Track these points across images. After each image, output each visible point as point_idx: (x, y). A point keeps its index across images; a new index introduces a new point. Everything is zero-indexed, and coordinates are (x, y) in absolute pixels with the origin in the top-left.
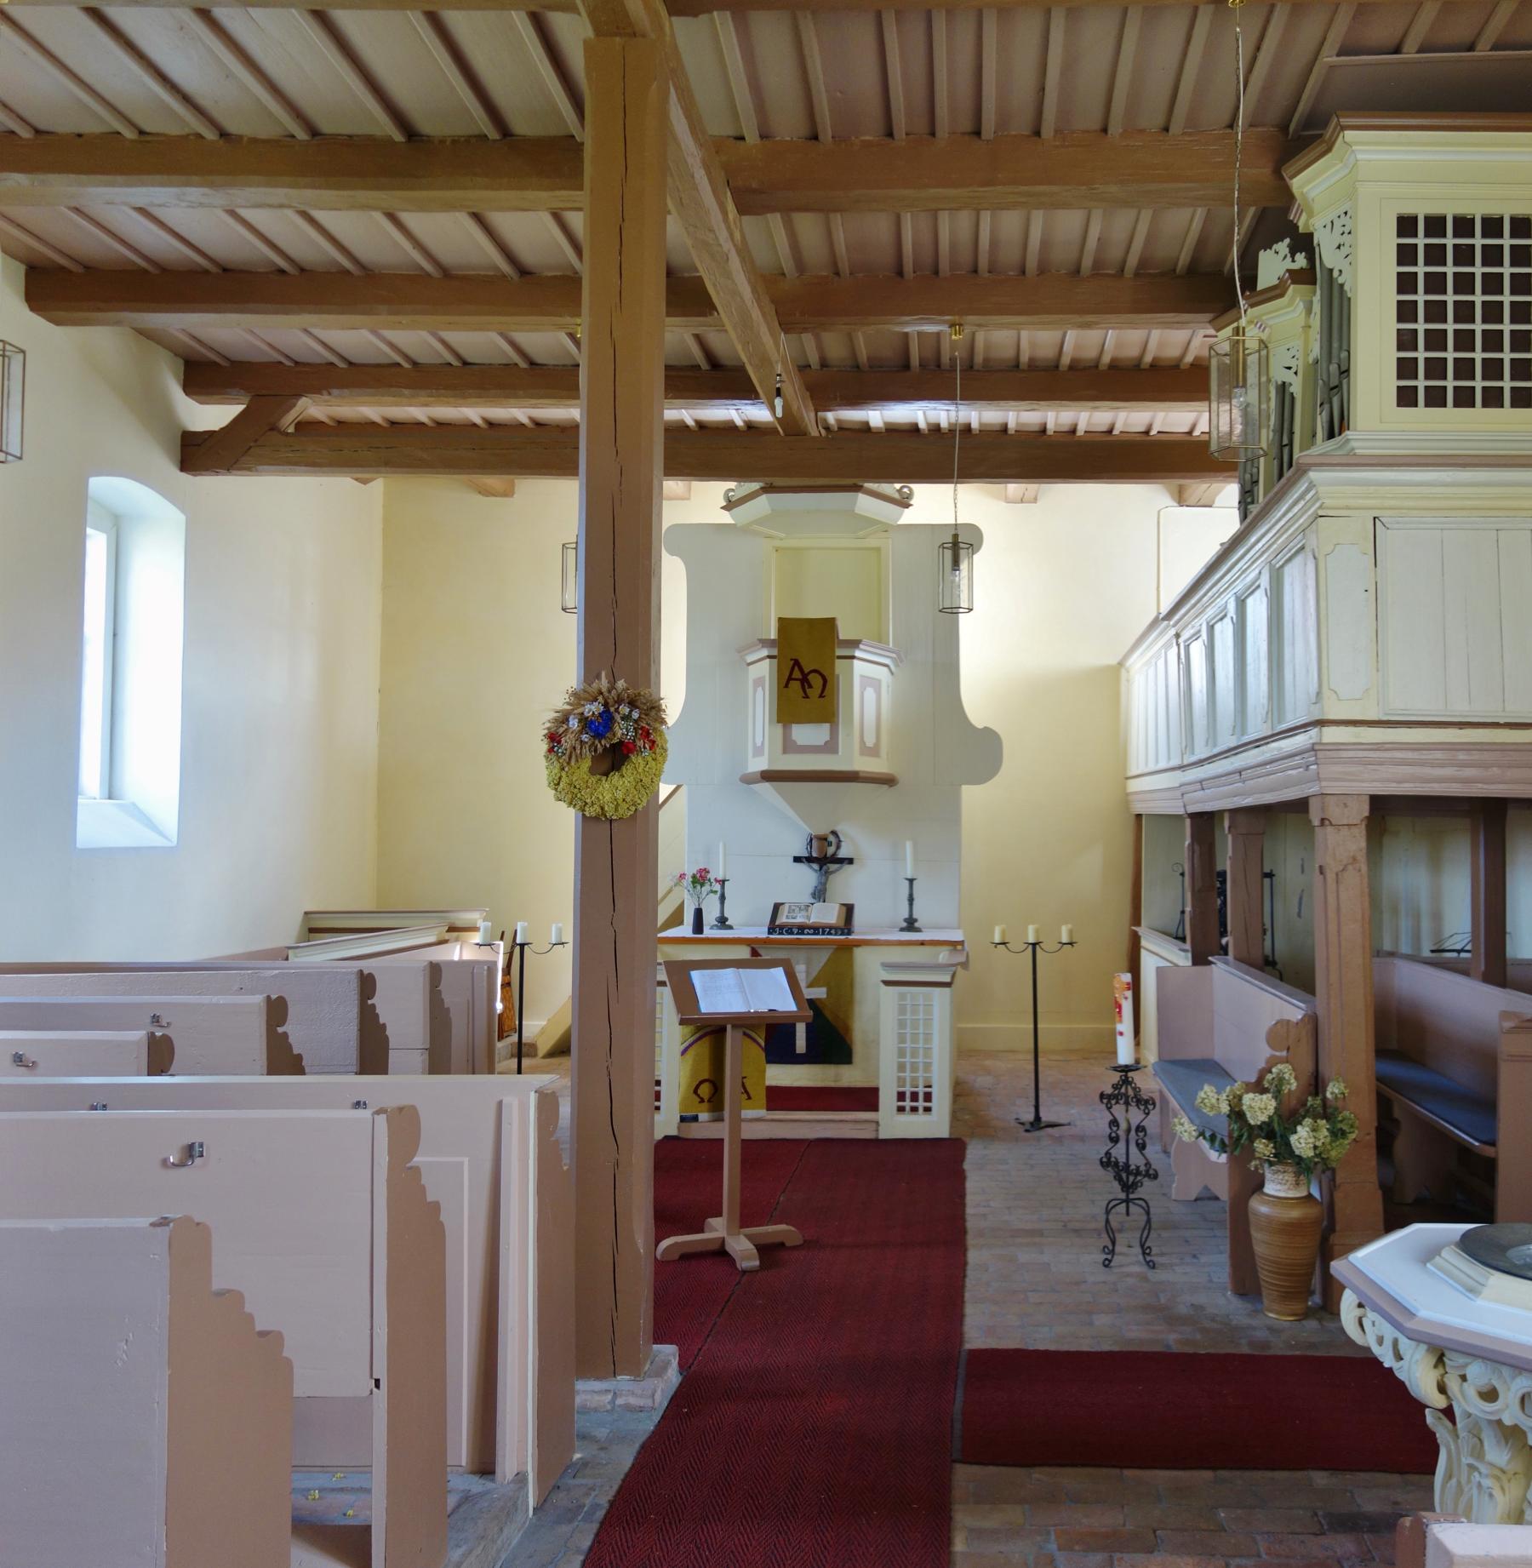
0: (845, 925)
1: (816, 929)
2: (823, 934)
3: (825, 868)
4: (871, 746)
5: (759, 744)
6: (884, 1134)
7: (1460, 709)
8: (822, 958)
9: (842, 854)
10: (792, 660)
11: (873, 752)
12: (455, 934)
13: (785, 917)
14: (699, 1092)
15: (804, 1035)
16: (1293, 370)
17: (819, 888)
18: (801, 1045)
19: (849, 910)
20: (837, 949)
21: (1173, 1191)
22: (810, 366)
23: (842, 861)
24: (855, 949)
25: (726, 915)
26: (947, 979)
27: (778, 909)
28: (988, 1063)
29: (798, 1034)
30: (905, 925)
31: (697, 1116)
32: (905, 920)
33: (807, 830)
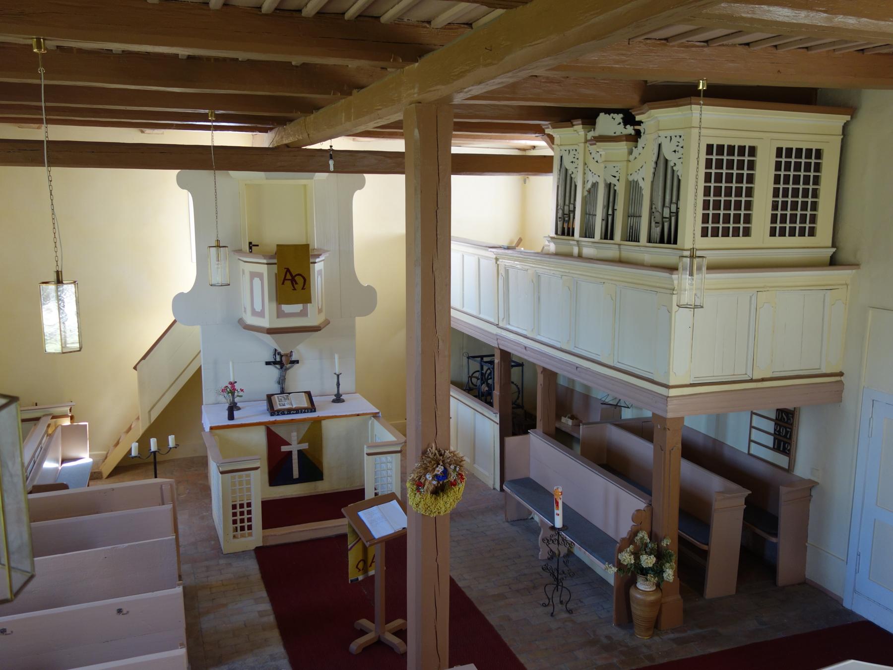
7: (726, 376)
16: (617, 178)
18: (296, 474)
21: (540, 556)
29: (294, 469)
31: (358, 578)
32: (335, 395)
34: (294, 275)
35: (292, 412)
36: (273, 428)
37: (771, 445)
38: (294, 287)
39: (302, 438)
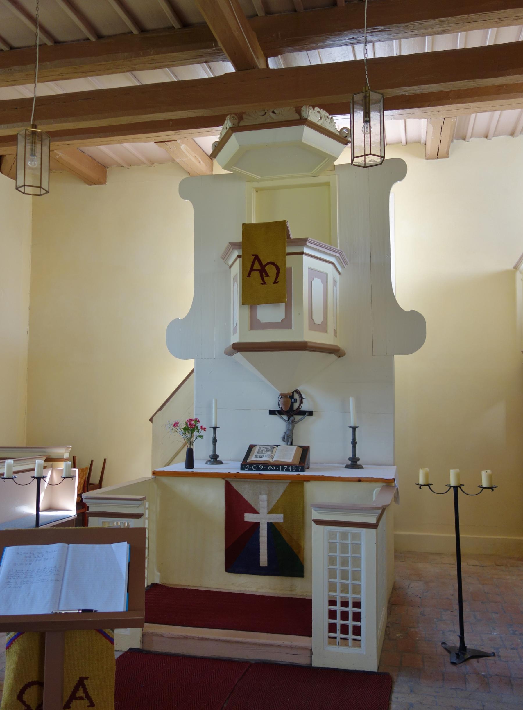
0: (300, 463)
1: (277, 466)
2: (283, 470)
3: (292, 418)
4: (320, 323)
5: (235, 325)
6: (317, 663)
8: (280, 489)
9: (304, 408)
10: (253, 255)
11: (323, 328)
12: (51, 463)
13: (254, 456)
14: (25, 697)
15: (266, 551)
17: (287, 433)
18: (264, 560)
19: (305, 451)
20: (290, 483)
22: (257, 15)
23: (303, 413)
24: (305, 483)
25: (217, 453)
26: (373, 520)
27: (252, 449)
28: (420, 565)
30: (350, 462)
33: (278, 393)
34: (264, 263)
35: (269, 468)
36: (235, 485)
37: (148, 585)
38: (263, 279)
39: (275, 506)
